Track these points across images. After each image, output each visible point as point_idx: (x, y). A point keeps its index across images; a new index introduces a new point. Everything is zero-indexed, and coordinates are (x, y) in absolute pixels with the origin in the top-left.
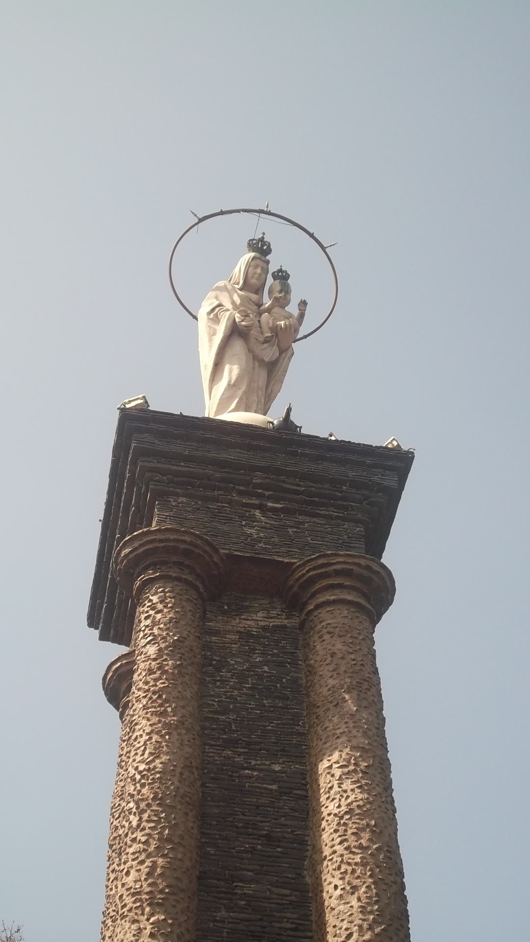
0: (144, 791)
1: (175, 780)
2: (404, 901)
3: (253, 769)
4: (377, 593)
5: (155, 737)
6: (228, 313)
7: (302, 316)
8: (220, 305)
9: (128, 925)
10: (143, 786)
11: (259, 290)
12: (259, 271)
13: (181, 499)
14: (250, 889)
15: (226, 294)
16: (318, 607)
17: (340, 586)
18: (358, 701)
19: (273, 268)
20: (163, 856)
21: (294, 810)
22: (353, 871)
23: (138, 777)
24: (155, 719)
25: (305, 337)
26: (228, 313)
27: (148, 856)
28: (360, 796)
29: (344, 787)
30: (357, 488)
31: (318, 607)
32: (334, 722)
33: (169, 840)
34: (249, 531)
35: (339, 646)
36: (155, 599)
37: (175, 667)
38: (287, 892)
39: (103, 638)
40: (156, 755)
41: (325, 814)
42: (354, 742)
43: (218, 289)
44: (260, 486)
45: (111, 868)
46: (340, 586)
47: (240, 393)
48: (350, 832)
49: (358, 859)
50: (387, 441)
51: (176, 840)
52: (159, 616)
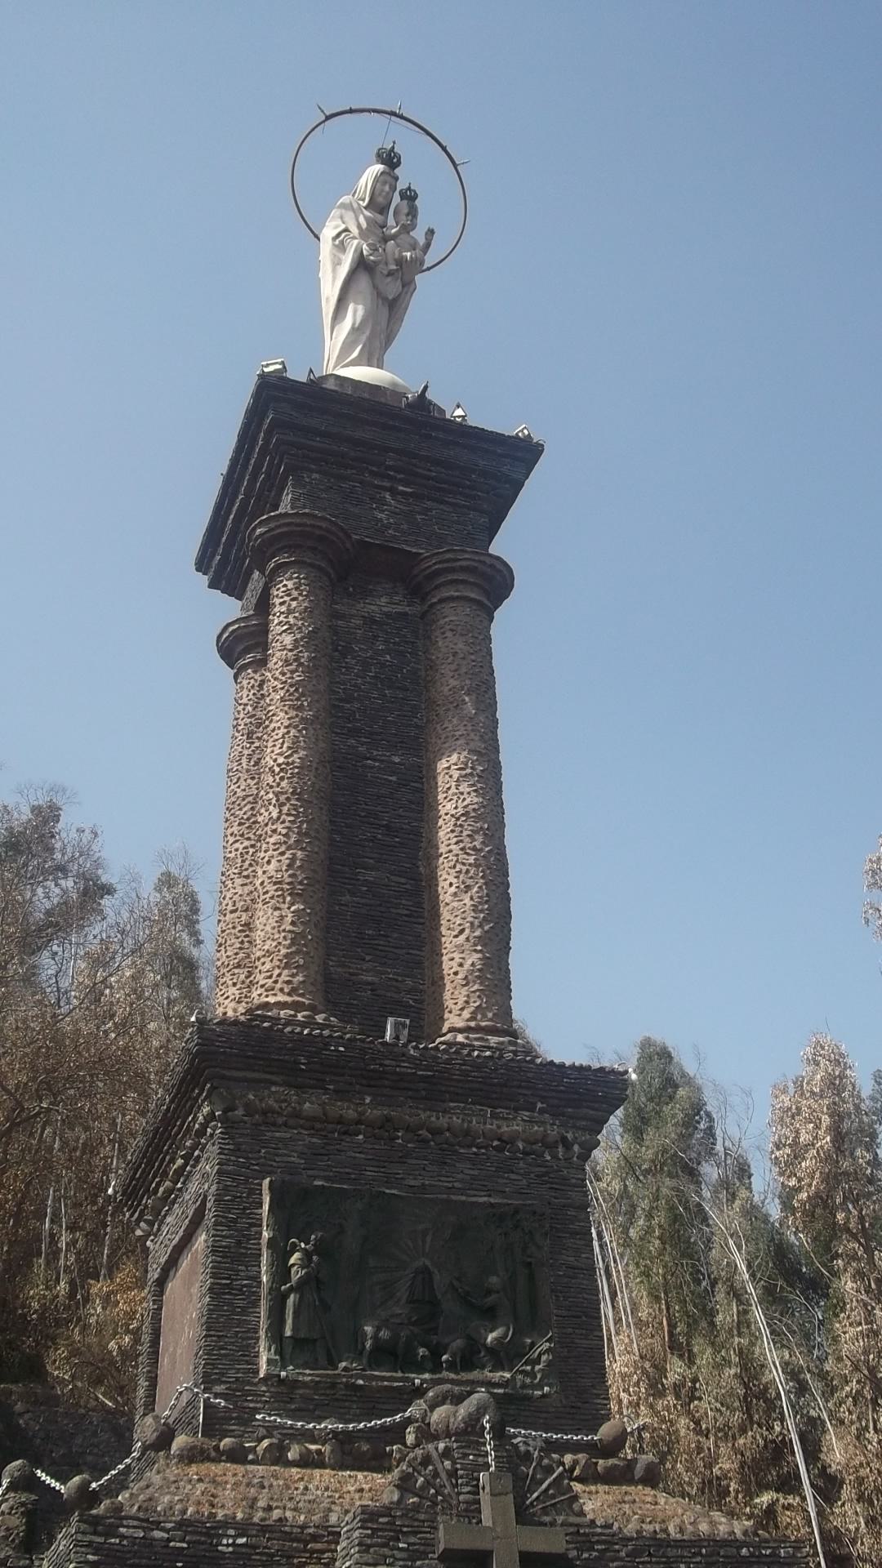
0: (284, 784)
1: (312, 775)
2: (509, 900)
3: (375, 760)
4: (496, 583)
5: (293, 732)
6: (356, 242)
7: (428, 246)
8: (346, 230)
9: (270, 911)
10: (282, 779)
11: (383, 210)
12: (387, 188)
13: (315, 476)
14: (371, 876)
15: (351, 214)
16: (441, 601)
17: (463, 582)
18: (477, 703)
19: (401, 185)
20: (302, 849)
21: (411, 802)
22: (467, 872)
23: (277, 769)
24: (293, 713)
25: (429, 269)
26: (356, 242)
27: (288, 849)
28: (476, 800)
29: (461, 789)
30: (479, 472)
31: (441, 601)
32: (452, 723)
33: (306, 834)
34: (380, 516)
35: (461, 645)
36: (290, 584)
37: (310, 659)
38: (403, 880)
39: (213, 585)
40: (294, 749)
41: (442, 812)
42: (472, 745)
43: (343, 206)
44: (390, 468)
45: (229, 831)
46: (463, 582)
47: (364, 338)
48: (465, 833)
49: (471, 860)
50: (518, 429)
51: (313, 833)
52: (294, 604)
